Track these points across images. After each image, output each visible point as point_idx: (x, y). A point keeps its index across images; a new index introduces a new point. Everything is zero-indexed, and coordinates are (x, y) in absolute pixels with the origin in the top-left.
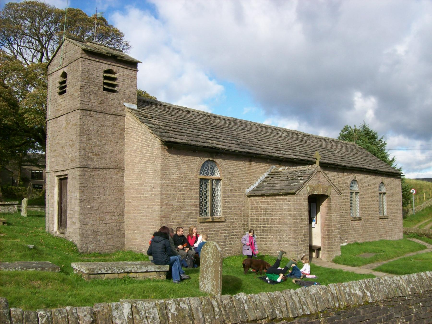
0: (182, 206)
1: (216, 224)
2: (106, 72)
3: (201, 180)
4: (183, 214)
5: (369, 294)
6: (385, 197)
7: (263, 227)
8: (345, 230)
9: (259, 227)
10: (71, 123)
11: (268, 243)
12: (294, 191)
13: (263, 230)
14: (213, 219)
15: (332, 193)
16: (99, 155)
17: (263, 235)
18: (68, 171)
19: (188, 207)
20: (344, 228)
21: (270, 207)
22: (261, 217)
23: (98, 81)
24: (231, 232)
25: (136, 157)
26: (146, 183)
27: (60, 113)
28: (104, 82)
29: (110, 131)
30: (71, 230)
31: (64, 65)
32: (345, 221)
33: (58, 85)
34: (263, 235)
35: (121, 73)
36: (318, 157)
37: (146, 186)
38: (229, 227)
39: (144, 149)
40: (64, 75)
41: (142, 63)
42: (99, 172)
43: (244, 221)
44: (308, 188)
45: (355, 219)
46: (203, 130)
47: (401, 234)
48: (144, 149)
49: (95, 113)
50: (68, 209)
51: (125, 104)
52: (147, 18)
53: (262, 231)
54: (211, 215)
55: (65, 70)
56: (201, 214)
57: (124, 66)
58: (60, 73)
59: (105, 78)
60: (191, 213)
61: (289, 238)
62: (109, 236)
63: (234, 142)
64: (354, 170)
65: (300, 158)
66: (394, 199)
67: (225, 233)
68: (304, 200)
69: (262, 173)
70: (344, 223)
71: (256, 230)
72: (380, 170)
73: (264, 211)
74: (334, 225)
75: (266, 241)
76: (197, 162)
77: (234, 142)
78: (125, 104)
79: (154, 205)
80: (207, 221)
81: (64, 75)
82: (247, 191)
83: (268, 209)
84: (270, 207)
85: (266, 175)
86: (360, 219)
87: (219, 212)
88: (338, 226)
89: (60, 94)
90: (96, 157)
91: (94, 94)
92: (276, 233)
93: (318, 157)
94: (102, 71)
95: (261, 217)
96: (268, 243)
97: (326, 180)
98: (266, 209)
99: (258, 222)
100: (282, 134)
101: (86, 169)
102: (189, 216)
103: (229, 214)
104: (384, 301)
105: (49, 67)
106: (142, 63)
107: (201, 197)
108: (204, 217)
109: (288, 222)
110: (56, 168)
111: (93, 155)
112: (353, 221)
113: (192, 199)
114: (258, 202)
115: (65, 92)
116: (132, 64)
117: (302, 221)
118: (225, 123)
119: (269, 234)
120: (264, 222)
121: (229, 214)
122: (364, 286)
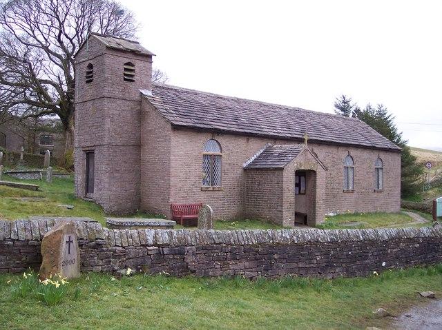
1: (216, 192)
2: (126, 64)
4: (189, 184)
14: (213, 188)
15: (319, 169)
19: (192, 178)
27: (87, 99)
30: (98, 195)
31: (90, 57)
33: (85, 74)
35: (139, 64)
36: (306, 138)
40: (90, 66)
45: (348, 192)
46: (207, 112)
50: (95, 178)
52: (231, 215)
58: (87, 63)
59: (125, 69)
63: (234, 123)
65: (295, 136)
69: (259, 150)
72: (377, 146)
76: (374, 156)
77: (234, 123)
81: (90, 66)
82: (244, 165)
85: (262, 151)
88: (324, 197)
89: (87, 82)
93: (306, 138)
100: (283, 113)
110: (83, 145)
115: (91, 81)
116: (148, 57)
118: (229, 104)
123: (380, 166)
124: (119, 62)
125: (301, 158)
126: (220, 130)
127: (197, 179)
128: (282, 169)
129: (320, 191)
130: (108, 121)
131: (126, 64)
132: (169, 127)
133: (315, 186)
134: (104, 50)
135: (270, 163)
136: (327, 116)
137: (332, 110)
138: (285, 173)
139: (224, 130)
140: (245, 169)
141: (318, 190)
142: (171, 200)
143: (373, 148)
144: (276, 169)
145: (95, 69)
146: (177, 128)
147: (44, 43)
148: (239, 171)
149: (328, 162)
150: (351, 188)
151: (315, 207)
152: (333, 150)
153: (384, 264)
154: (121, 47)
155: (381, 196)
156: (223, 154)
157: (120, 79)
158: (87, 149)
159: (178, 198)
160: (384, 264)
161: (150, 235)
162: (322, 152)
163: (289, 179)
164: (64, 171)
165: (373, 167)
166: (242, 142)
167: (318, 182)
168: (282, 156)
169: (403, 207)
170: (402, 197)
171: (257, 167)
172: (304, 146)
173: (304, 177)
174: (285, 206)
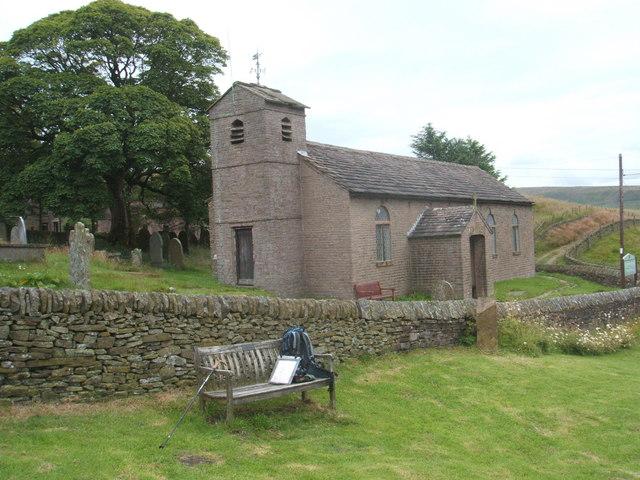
15: (486, 233)
33: (230, 134)
36: (475, 198)
55: (240, 118)
58: (234, 119)
76: (374, 208)
82: (408, 234)
93: (475, 198)
109: (454, 263)
110: (233, 219)
116: (298, 109)
124: (274, 119)
126: (387, 194)
128: (459, 236)
130: (272, 190)
131: (283, 120)
132: (346, 194)
133: (484, 253)
136: (407, 160)
137: (409, 152)
138: (462, 239)
142: (354, 280)
144: (450, 236)
145: (246, 128)
148: (404, 241)
154: (277, 100)
159: (359, 280)
163: (465, 244)
167: (487, 247)
168: (453, 221)
171: (426, 234)
172: (474, 208)
173: (477, 240)
174: (465, 277)
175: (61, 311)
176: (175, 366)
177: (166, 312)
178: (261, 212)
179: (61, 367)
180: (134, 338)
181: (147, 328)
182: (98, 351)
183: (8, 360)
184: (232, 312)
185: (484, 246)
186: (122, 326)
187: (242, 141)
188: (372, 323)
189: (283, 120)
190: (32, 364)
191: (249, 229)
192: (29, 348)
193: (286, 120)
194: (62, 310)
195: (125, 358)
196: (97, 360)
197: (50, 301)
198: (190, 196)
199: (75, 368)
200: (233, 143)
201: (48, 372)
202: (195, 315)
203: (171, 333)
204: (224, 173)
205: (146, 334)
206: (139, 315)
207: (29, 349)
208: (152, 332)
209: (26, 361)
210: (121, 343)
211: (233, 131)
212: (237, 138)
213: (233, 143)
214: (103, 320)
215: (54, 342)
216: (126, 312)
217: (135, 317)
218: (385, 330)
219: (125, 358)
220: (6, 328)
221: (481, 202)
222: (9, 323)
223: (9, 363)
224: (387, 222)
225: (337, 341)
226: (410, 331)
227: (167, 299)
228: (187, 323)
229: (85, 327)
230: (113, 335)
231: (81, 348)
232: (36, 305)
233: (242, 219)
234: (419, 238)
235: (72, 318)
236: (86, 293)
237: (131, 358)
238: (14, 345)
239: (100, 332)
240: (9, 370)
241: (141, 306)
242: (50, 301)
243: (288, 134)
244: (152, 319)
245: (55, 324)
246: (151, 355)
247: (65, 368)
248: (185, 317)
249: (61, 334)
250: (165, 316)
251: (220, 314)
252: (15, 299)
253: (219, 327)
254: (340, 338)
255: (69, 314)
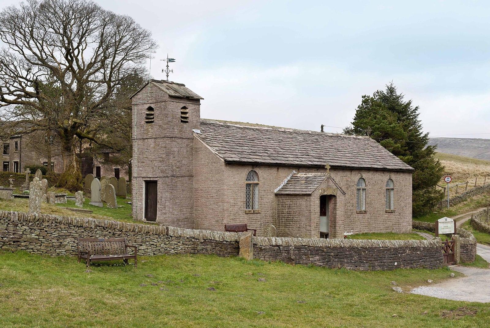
0: (236, 203)
1: (255, 215)
3: (248, 185)
4: (236, 208)
5: (342, 244)
6: (392, 193)
7: (287, 217)
8: (351, 221)
9: (284, 217)
10: (160, 145)
11: (290, 229)
12: (310, 193)
13: (287, 219)
15: (339, 194)
16: (179, 168)
17: (287, 223)
18: (158, 178)
19: (239, 203)
20: (350, 219)
21: (293, 203)
22: (286, 210)
23: (177, 116)
24: (264, 221)
25: (204, 169)
26: (212, 187)
28: (181, 116)
29: (185, 151)
32: (352, 214)
33: (145, 116)
34: (287, 223)
35: (191, 107)
37: (213, 189)
38: (263, 217)
39: (211, 164)
41: (204, 99)
42: (179, 179)
43: (273, 213)
44: (320, 191)
45: (361, 213)
47: (411, 227)
48: (211, 164)
49: (177, 139)
51: (193, 130)
53: (286, 220)
54: (252, 209)
55: (152, 106)
56: (246, 208)
57: (191, 103)
58: (148, 105)
60: (241, 207)
61: (306, 226)
62: (186, 223)
64: (363, 169)
66: (403, 194)
67: (261, 221)
68: (317, 199)
69: (286, 177)
70: (351, 216)
71: (282, 219)
72: (388, 167)
73: (288, 206)
74: (339, 217)
75: (289, 227)
76: (245, 172)
78: (193, 130)
79: (219, 202)
80: (251, 212)
82: (276, 191)
83: (291, 205)
84: (293, 203)
85: (289, 178)
86: (365, 212)
87: (256, 207)
90: (178, 169)
91: (176, 126)
92: (297, 222)
94: (180, 108)
95: (286, 210)
96: (290, 229)
97: (334, 184)
98: (289, 205)
99: (284, 213)
101: (173, 178)
102: (240, 209)
103: (264, 208)
104: (349, 248)
105: (132, 98)
106: (204, 99)
107: (246, 196)
108: (248, 210)
109: (306, 215)
110: (144, 175)
111: (176, 168)
112: (359, 215)
113: (241, 198)
114: (283, 199)
116: (196, 100)
117: (316, 214)
119: (291, 223)
120: (288, 213)
121: (264, 208)
122: (340, 241)
123: (392, 187)
124: (176, 107)
125: (317, 184)
127: (242, 203)
129: (340, 212)
131: (182, 108)
133: (335, 209)
134: (166, 98)
135: (298, 189)
139: (261, 163)
140: (276, 195)
141: (338, 212)
143: (384, 170)
145: (156, 112)
146: (229, 163)
147: (38, 53)
149: (342, 185)
150: (363, 209)
151: (335, 227)
152: (348, 174)
153: (396, 264)
155: (392, 215)
156: (260, 183)
157: (178, 121)
158: (149, 179)
160: (396, 264)
161: (480, 210)
162: (338, 177)
164: (67, 193)
165: (385, 188)
166: (273, 171)
167: (338, 205)
169: (415, 227)
170: (413, 217)
175: (26, 221)
176: (72, 246)
177: (69, 225)
178: (162, 171)
179: (25, 242)
180: (55, 233)
181: (61, 230)
182: (40, 237)
183: (5, 237)
184: (99, 226)
185: (335, 204)
186: (50, 228)
187: (152, 122)
188: (174, 238)
189: (182, 108)
190: (14, 240)
191: (156, 182)
192: (13, 233)
193: (184, 108)
194: (27, 221)
195: (51, 241)
196: (39, 240)
197: (22, 217)
198: (117, 153)
199: (30, 243)
200: (147, 122)
201: (20, 243)
202: (82, 226)
203: (71, 233)
204: (140, 142)
205: (60, 232)
206: (58, 224)
207: (14, 234)
208: (62, 231)
209: (12, 238)
210: (49, 235)
211: (147, 115)
212: (149, 119)
213: (147, 122)
214: (43, 225)
215: (23, 232)
216: (52, 223)
217: (56, 225)
218: (181, 242)
219: (51, 241)
220: (6, 225)
221: (334, 168)
222: (7, 224)
223: (6, 238)
224: (256, 182)
225: (153, 244)
226: (198, 245)
227: (70, 219)
228: (78, 229)
229: (35, 227)
230: (46, 231)
231: (33, 235)
232: (17, 218)
233: (151, 175)
234: (282, 195)
235: (30, 224)
236: (37, 215)
237: (53, 241)
238: (8, 232)
239: (41, 230)
240: (5, 241)
241: (58, 221)
242: (22, 217)
243: (186, 118)
244: (62, 226)
245: (24, 225)
246: (61, 241)
247: (27, 242)
248: (77, 227)
249: (26, 229)
250: (69, 226)
251: (93, 227)
252: (9, 215)
253: (93, 232)
254: (154, 243)
255: (30, 222)
